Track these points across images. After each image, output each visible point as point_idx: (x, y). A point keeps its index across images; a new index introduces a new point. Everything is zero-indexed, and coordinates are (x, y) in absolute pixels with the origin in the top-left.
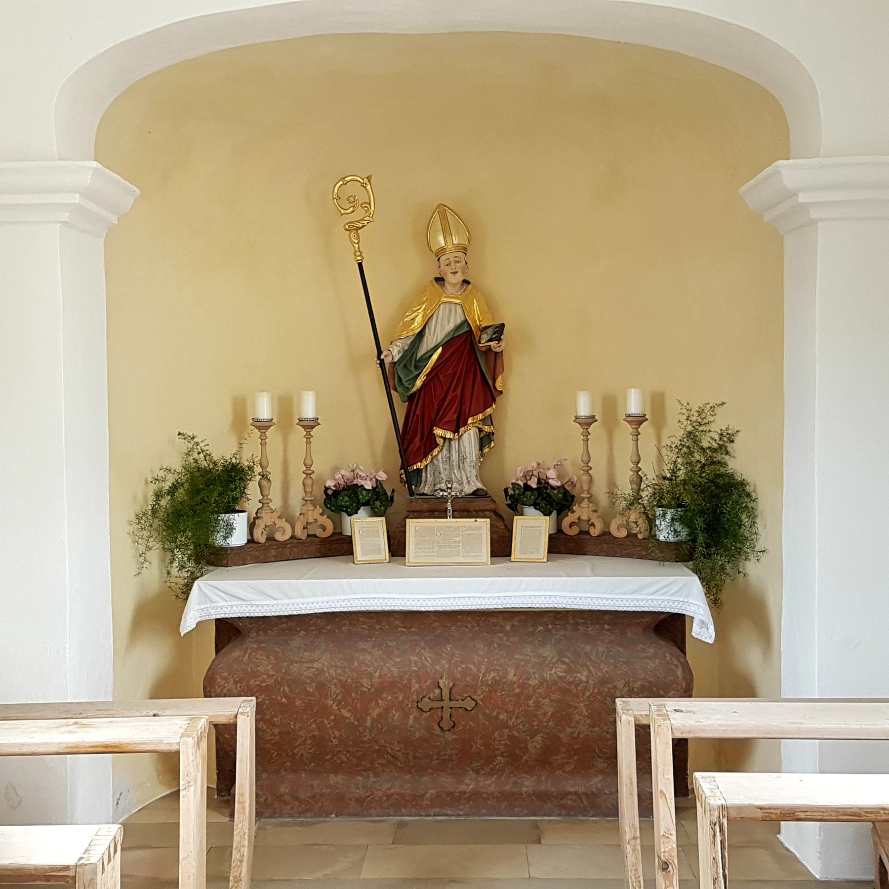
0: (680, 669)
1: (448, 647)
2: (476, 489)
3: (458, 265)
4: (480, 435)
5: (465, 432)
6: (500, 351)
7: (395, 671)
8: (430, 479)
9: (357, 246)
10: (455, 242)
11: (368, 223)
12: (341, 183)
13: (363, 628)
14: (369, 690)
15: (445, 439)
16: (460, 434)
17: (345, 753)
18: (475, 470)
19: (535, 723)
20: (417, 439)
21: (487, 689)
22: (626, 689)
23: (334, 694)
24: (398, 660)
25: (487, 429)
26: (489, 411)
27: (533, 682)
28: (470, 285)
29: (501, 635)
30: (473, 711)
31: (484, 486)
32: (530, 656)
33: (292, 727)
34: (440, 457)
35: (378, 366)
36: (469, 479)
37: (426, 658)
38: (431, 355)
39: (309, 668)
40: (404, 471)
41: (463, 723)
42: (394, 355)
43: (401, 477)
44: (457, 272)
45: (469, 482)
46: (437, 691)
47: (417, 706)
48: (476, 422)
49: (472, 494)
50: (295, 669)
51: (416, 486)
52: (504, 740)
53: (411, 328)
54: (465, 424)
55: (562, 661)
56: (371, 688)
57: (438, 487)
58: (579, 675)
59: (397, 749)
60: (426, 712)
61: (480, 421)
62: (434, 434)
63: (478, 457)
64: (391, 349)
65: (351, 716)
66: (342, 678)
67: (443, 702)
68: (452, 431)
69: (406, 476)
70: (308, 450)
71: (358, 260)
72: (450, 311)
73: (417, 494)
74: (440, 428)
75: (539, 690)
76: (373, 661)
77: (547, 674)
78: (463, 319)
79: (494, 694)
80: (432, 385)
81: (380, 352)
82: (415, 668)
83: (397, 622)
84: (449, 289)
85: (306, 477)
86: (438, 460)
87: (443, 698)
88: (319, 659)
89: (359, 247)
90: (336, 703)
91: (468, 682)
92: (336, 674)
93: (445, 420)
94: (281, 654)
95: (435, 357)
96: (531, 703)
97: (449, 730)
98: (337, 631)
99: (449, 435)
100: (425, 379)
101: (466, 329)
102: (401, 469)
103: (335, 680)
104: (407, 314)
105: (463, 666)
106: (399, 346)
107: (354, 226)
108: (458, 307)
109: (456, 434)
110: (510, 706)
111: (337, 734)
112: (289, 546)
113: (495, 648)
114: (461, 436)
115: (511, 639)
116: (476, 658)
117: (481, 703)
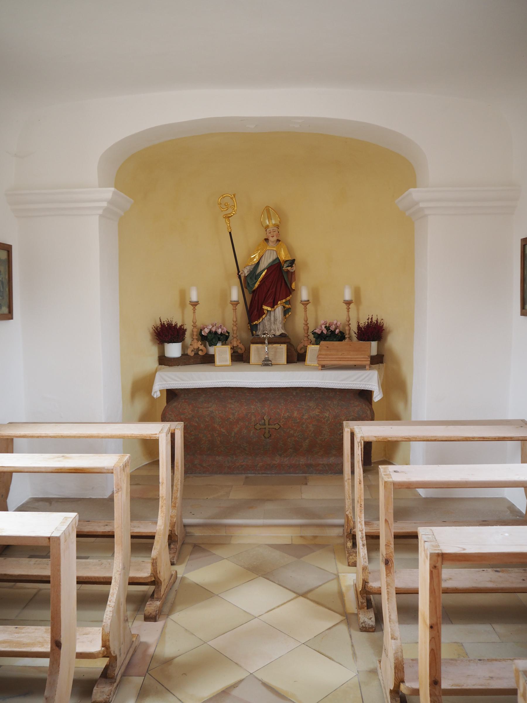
0: (369, 411)
1: (268, 402)
2: (281, 333)
3: (274, 233)
4: (284, 309)
5: (277, 308)
8: (261, 328)
9: (228, 225)
11: (234, 214)
12: (222, 197)
15: (268, 311)
16: (275, 308)
17: (223, 447)
20: (256, 311)
24: (246, 407)
25: (287, 306)
26: (288, 298)
28: (280, 242)
29: (291, 397)
30: (279, 430)
32: (304, 406)
34: (266, 318)
35: (238, 278)
38: (262, 273)
41: (274, 435)
42: (245, 273)
45: (278, 330)
46: (263, 421)
47: (254, 427)
49: (279, 335)
50: (201, 411)
52: (292, 442)
54: (277, 304)
58: (325, 414)
61: (284, 302)
62: (263, 308)
64: (244, 270)
67: (266, 426)
72: (271, 253)
75: (307, 421)
78: (276, 257)
81: (239, 271)
83: (246, 391)
88: (211, 407)
89: (229, 225)
90: (219, 426)
92: (219, 413)
94: (194, 405)
95: (264, 273)
96: (304, 426)
97: (268, 438)
98: (219, 395)
99: (269, 309)
101: (278, 261)
102: (248, 324)
105: (275, 410)
109: (273, 308)
111: (219, 439)
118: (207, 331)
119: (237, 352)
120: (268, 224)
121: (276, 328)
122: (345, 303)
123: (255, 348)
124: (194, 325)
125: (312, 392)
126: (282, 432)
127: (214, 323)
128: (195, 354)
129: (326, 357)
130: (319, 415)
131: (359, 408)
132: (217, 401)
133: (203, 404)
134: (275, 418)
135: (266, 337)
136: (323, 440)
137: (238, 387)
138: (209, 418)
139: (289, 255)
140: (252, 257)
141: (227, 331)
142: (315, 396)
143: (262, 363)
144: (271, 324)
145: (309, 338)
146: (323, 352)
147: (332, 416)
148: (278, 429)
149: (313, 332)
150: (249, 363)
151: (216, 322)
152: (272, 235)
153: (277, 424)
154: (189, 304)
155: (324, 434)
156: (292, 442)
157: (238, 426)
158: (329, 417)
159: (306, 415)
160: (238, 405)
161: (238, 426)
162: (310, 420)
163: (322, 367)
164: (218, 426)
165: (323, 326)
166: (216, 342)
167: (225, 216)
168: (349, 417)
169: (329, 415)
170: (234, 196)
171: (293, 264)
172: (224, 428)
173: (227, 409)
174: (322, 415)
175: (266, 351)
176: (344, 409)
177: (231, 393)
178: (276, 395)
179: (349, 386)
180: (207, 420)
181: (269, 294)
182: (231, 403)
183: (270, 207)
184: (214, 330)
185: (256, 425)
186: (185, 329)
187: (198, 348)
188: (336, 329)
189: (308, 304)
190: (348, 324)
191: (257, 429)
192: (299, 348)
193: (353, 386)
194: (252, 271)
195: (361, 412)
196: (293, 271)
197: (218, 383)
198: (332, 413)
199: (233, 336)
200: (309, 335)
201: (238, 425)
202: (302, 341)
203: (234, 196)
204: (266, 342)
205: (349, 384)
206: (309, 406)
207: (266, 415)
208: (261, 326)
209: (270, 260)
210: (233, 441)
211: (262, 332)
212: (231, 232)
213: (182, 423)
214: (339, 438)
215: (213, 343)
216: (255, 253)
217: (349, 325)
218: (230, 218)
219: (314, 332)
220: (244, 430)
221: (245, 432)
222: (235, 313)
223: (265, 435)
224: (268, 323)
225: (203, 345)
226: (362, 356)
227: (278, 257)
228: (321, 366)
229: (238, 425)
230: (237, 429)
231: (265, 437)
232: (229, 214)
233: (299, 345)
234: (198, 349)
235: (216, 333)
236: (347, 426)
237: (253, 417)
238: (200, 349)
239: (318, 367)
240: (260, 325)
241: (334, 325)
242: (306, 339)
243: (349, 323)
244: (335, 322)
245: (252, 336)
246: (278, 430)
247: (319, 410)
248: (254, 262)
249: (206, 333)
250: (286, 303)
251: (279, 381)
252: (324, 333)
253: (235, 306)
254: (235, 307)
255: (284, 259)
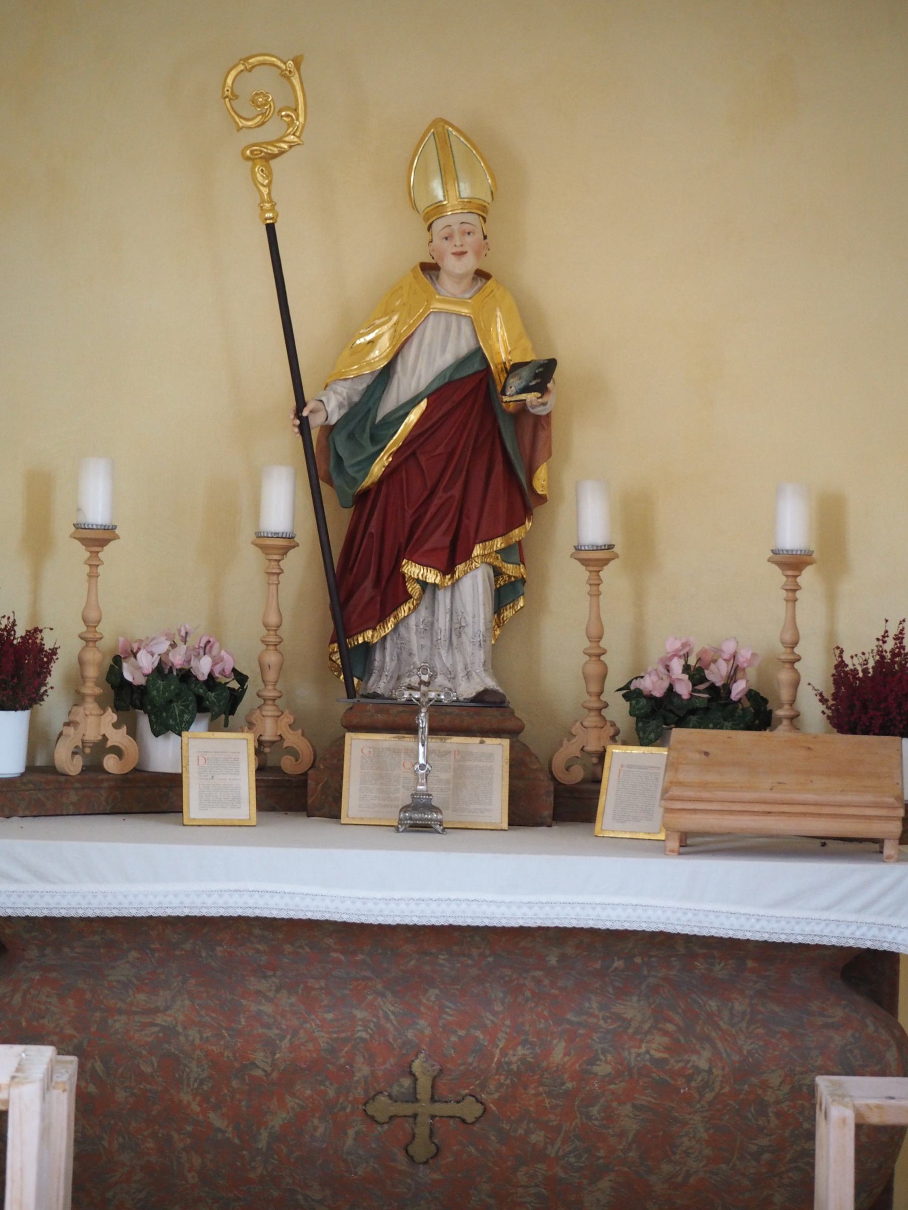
0: (894, 1049)
1: (433, 993)
2: (481, 689)
3: (469, 239)
4: (496, 581)
5: (466, 573)
6: (544, 413)
7: (323, 1038)
8: (390, 664)
9: (265, 191)
10: (464, 195)
11: (290, 147)
12: (241, 67)
13: (258, 951)
14: (268, 1075)
15: (424, 584)
16: (456, 576)
17: (210, 1201)
18: (482, 651)
19: (601, 1153)
20: (368, 583)
21: (508, 1081)
22: (786, 1089)
23: (195, 1081)
24: (329, 1016)
25: (510, 569)
26: (517, 534)
27: (603, 1069)
28: (490, 282)
29: (538, 974)
30: (477, 1125)
31: (500, 681)
32: (597, 1017)
33: (106, 1144)
34: (412, 621)
35: (296, 430)
36: (470, 669)
37: (385, 1013)
38: (406, 415)
39: (145, 1025)
40: (339, 647)
41: (455, 1148)
42: (329, 409)
43: (331, 659)
44: (466, 252)
45: (468, 675)
46: (407, 1082)
47: (365, 1110)
48: (490, 554)
49: (474, 700)
50: (117, 1025)
51: (360, 679)
52: (537, 1186)
53: (368, 359)
54: (467, 556)
55: (661, 1030)
56: (273, 1071)
57: (406, 681)
58: (694, 1058)
59: (318, 1197)
60: (381, 1124)
61: (497, 552)
62: (403, 575)
63: (490, 626)
64: (324, 399)
65: (227, 1127)
66: (214, 1048)
67: (417, 1105)
68: (440, 570)
69: (341, 657)
70: (92, 590)
71: (266, 219)
72: (448, 329)
73: (363, 696)
74: (416, 562)
75: (612, 1087)
76: (279, 1018)
77: (630, 1053)
78: (472, 345)
79: (523, 1091)
80: (404, 476)
81: (301, 403)
82: (364, 1035)
83: (330, 941)
84: (447, 284)
85: (87, 646)
86: (408, 628)
87: (419, 1097)
88: (167, 1008)
89: (269, 194)
90: (198, 1098)
91: (471, 1064)
92: (201, 1039)
93: (427, 546)
94: (88, 996)
95: (413, 417)
96: (595, 1111)
97: (426, 1163)
98: (204, 954)
99: (432, 577)
100: (390, 463)
101: (476, 366)
102: (332, 642)
103: (198, 1052)
104: (362, 331)
105: (462, 1033)
106: (340, 394)
107: (262, 152)
108: (464, 321)
109: (448, 577)
110: (552, 1117)
111: (197, 1161)
112: (105, 785)
113: (527, 1000)
114: (457, 580)
115: (560, 983)
116: (488, 1018)
117: (494, 1108)
118: (146, 662)
119: (278, 770)
120: (441, 197)
121: (460, 667)
122: (778, 563)
123: (366, 751)
124: (90, 636)
125: (635, 956)
126: (493, 1138)
127: (179, 631)
128: (85, 769)
129: (705, 795)
130: (664, 1061)
131: (849, 1033)
132: (193, 981)
133: (131, 992)
134: (462, 1067)
135: (424, 700)
136: (679, 1179)
137: (300, 920)
138: (154, 1059)
139: (526, 343)
140: (358, 342)
141: (234, 670)
142: (645, 972)
143: (400, 820)
144: (434, 644)
145: (604, 718)
146: (688, 775)
147: (723, 1069)
148: (473, 1123)
149: (627, 687)
150: (338, 817)
151: (187, 626)
152: (459, 250)
153: (473, 1099)
154: (73, 536)
155: (685, 1152)
156: (537, 1186)
157: (290, 1102)
158: (710, 1072)
159: (606, 1062)
160: (292, 1005)
161: (290, 1102)
162: (623, 1084)
163: (681, 846)
164: (194, 1100)
165: (677, 666)
166: (186, 717)
167: (252, 152)
168: (802, 1073)
169: (710, 1061)
170: (297, 65)
171: (549, 382)
172: (224, 1110)
173: (243, 1021)
174: (681, 1065)
175: (422, 761)
176: (778, 1036)
177: (261, 947)
178: (470, 962)
179: (808, 930)
180: (143, 1068)
181: (432, 510)
182: (258, 993)
183: (451, 125)
184: (177, 659)
185: (373, 1098)
186: (47, 648)
187: (101, 741)
188: (732, 677)
189: (606, 562)
190: (791, 657)
191: (378, 1119)
192: (559, 761)
193: (826, 932)
194: (357, 404)
195: (856, 1052)
196: (541, 411)
197: (209, 896)
198: (724, 1055)
199: (258, 695)
200: (606, 705)
201: (288, 1098)
202: (573, 731)
203: (297, 65)
204: (423, 721)
205: (808, 920)
206: (618, 1017)
207: (422, 1056)
208: (388, 652)
209: (445, 359)
210: (259, 1170)
211: (393, 681)
212: (276, 226)
213: (72, 1062)
214: (752, 1171)
215: (171, 722)
216: (378, 322)
217: (792, 663)
218: (273, 163)
219: (632, 687)
220: (316, 1121)
221: (318, 1134)
222: (273, 588)
223: (410, 1149)
224: (423, 642)
225: (124, 729)
226: (869, 798)
227: (479, 349)
228: (676, 837)
229: (288, 1098)
230: (284, 1115)
231: (411, 1158)
232: (269, 143)
233: (561, 745)
234: (101, 747)
235: (186, 676)
236: (840, 1097)
237: (359, 1059)
238: (109, 744)
239: (662, 843)
240: (384, 648)
241: (725, 660)
242: (592, 720)
243: (793, 653)
244: (729, 648)
245: (349, 697)
246: (476, 1128)
247: (666, 1040)
248: (369, 364)
249: (145, 675)
250: (505, 553)
251: (489, 898)
252: (679, 696)
253: (277, 557)
254: (279, 561)
255: (504, 357)
